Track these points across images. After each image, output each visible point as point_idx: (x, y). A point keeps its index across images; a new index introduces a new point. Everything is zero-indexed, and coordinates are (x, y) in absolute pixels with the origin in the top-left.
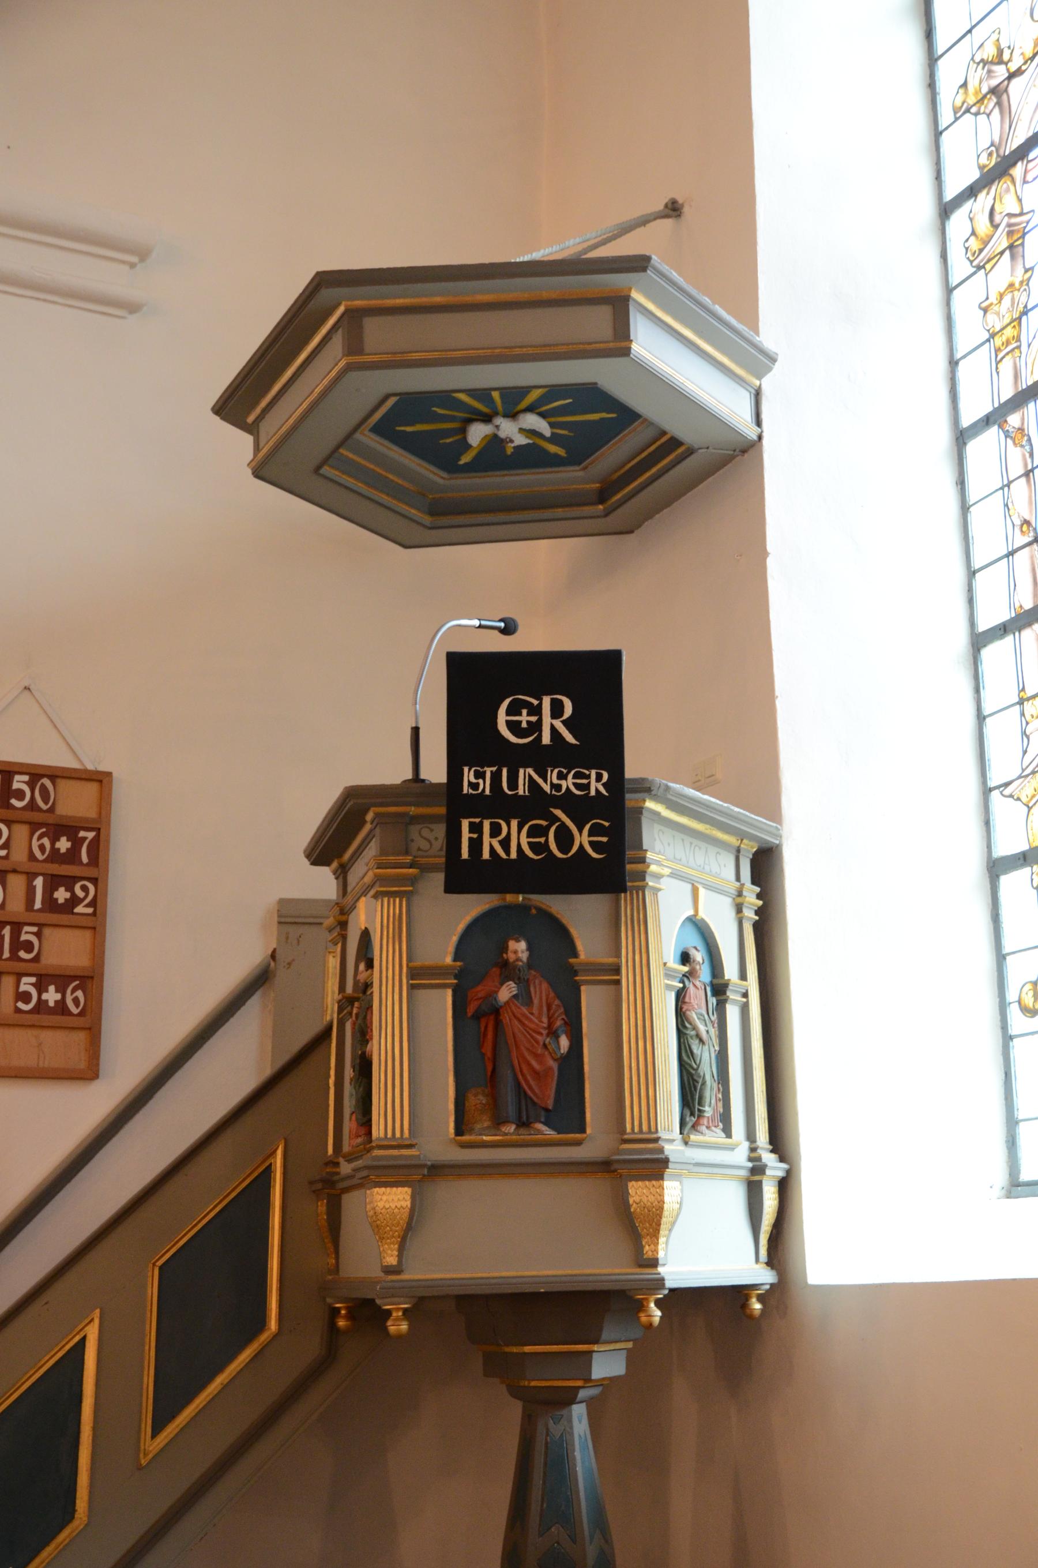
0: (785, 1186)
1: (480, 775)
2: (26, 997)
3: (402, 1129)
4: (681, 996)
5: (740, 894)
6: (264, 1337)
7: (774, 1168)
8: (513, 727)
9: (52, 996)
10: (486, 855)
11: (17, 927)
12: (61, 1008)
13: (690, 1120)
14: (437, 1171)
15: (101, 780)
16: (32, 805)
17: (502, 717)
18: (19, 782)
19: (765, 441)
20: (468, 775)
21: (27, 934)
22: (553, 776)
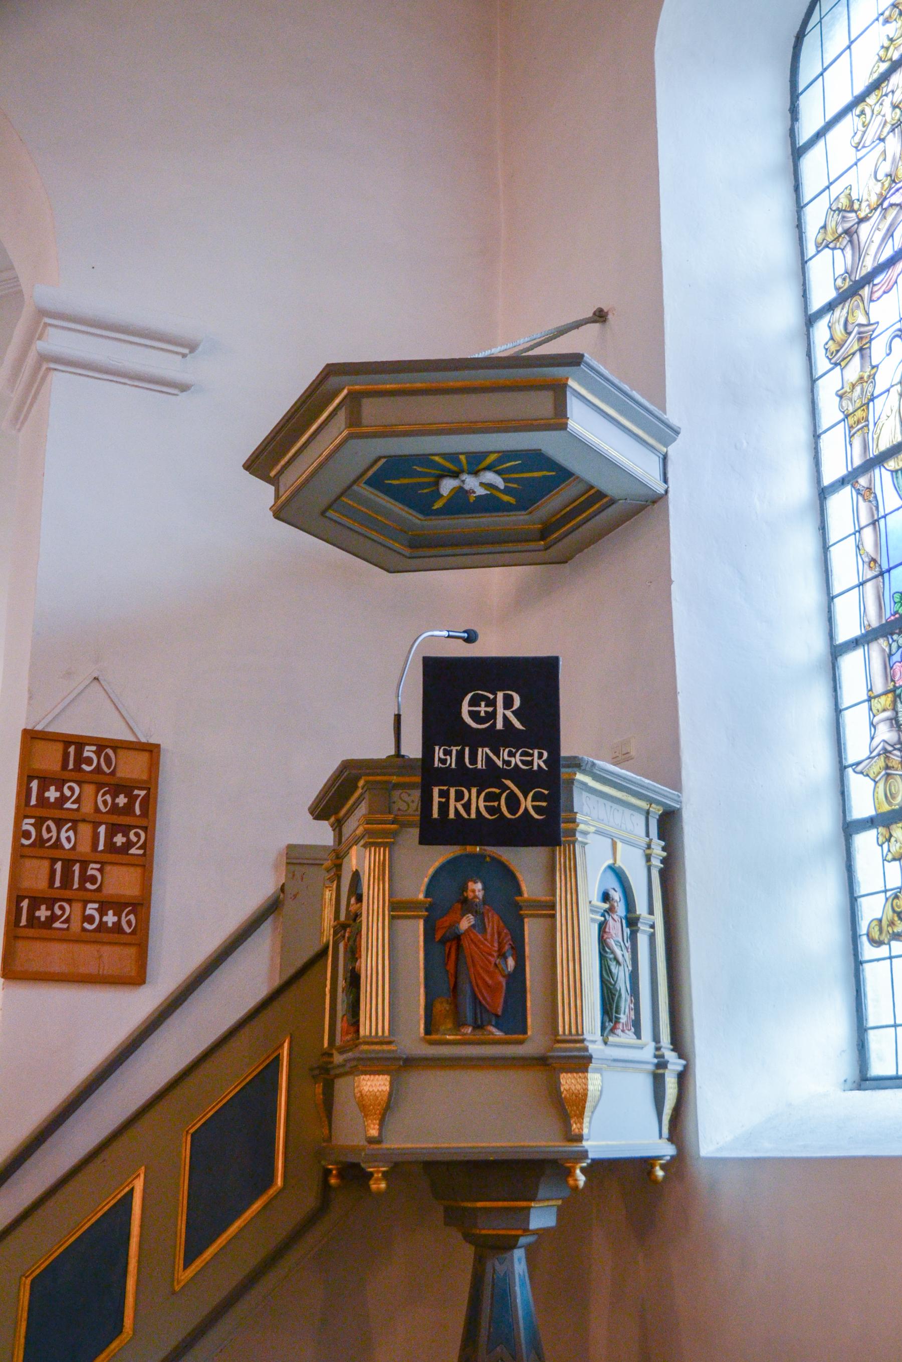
0: (683, 1078)
1: (447, 753)
2: (90, 919)
6: (272, 1192)
7: (675, 1064)
8: (474, 715)
9: (110, 919)
10: (452, 815)
11: (84, 865)
12: (117, 928)
14: (410, 1063)
15: (152, 751)
16: (98, 770)
17: (465, 708)
18: (89, 752)
20: (439, 753)
21: (93, 870)
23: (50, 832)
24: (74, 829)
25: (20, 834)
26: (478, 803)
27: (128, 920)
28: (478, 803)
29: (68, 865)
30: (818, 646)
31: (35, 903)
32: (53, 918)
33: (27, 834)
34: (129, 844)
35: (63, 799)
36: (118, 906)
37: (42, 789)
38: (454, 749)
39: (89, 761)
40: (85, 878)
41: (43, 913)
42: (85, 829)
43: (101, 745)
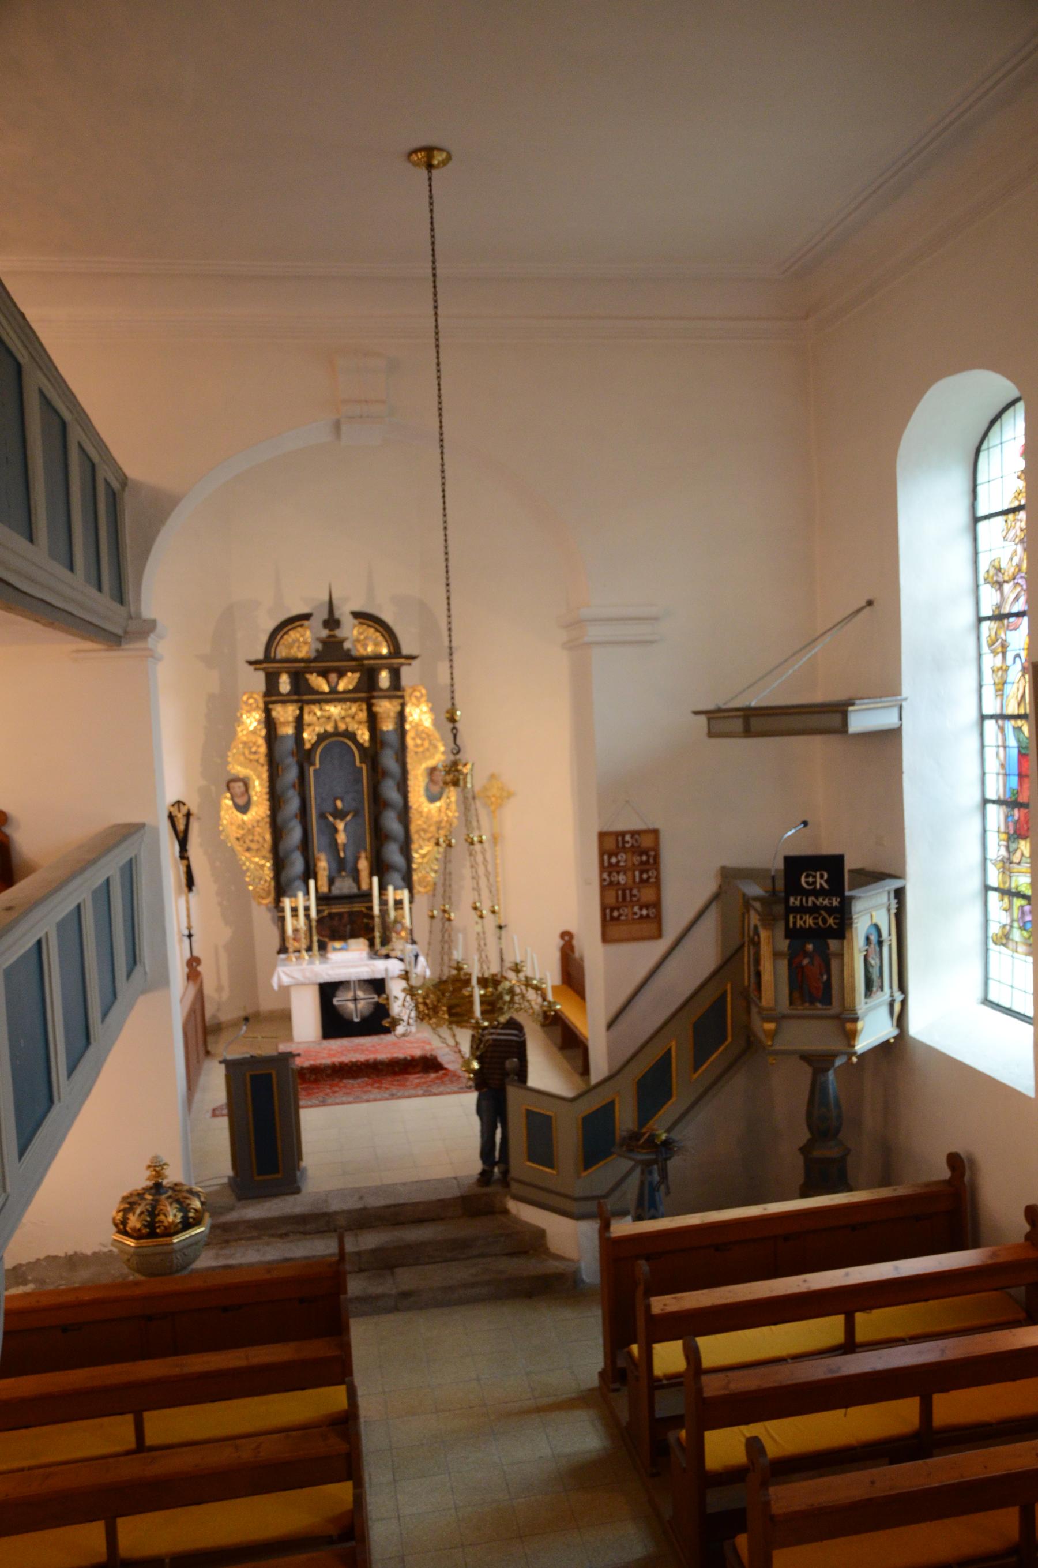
0: (904, 1003)
1: (796, 899)
2: (635, 914)
3: (772, 1004)
4: (866, 958)
5: (889, 905)
6: (727, 1043)
7: (899, 997)
8: (807, 883)
9: (644, 912)
10: (798, 926)
11: (631, 890)
12: (648, 916)
13: (869, 993)
14: (784, 1017)
15: (655, 832)
16: (633, 846)
17: (803, 880)
18: (628, 838)
19: (904, 727)
20: (792, 900)
21: (635, 892)
22: (821, 899)
23: (615, 878)
24: (625, 874)
25: (602, 880)
26: (809, 921)
27: (652, 912)
28: (809, 921)
29: (624, 891)
30: (977, 798)
31: (612, 910)
32: (620, 915)
33: (605, 880)
34: (649, 878)
35: (618, 862)
36: (647, 907)
37: (610, 858)
38: (799, 898)
39: (628, 842)
40: (632, 896)
41: (616, 914)
42: (630, 874)
43: (634, 833)
